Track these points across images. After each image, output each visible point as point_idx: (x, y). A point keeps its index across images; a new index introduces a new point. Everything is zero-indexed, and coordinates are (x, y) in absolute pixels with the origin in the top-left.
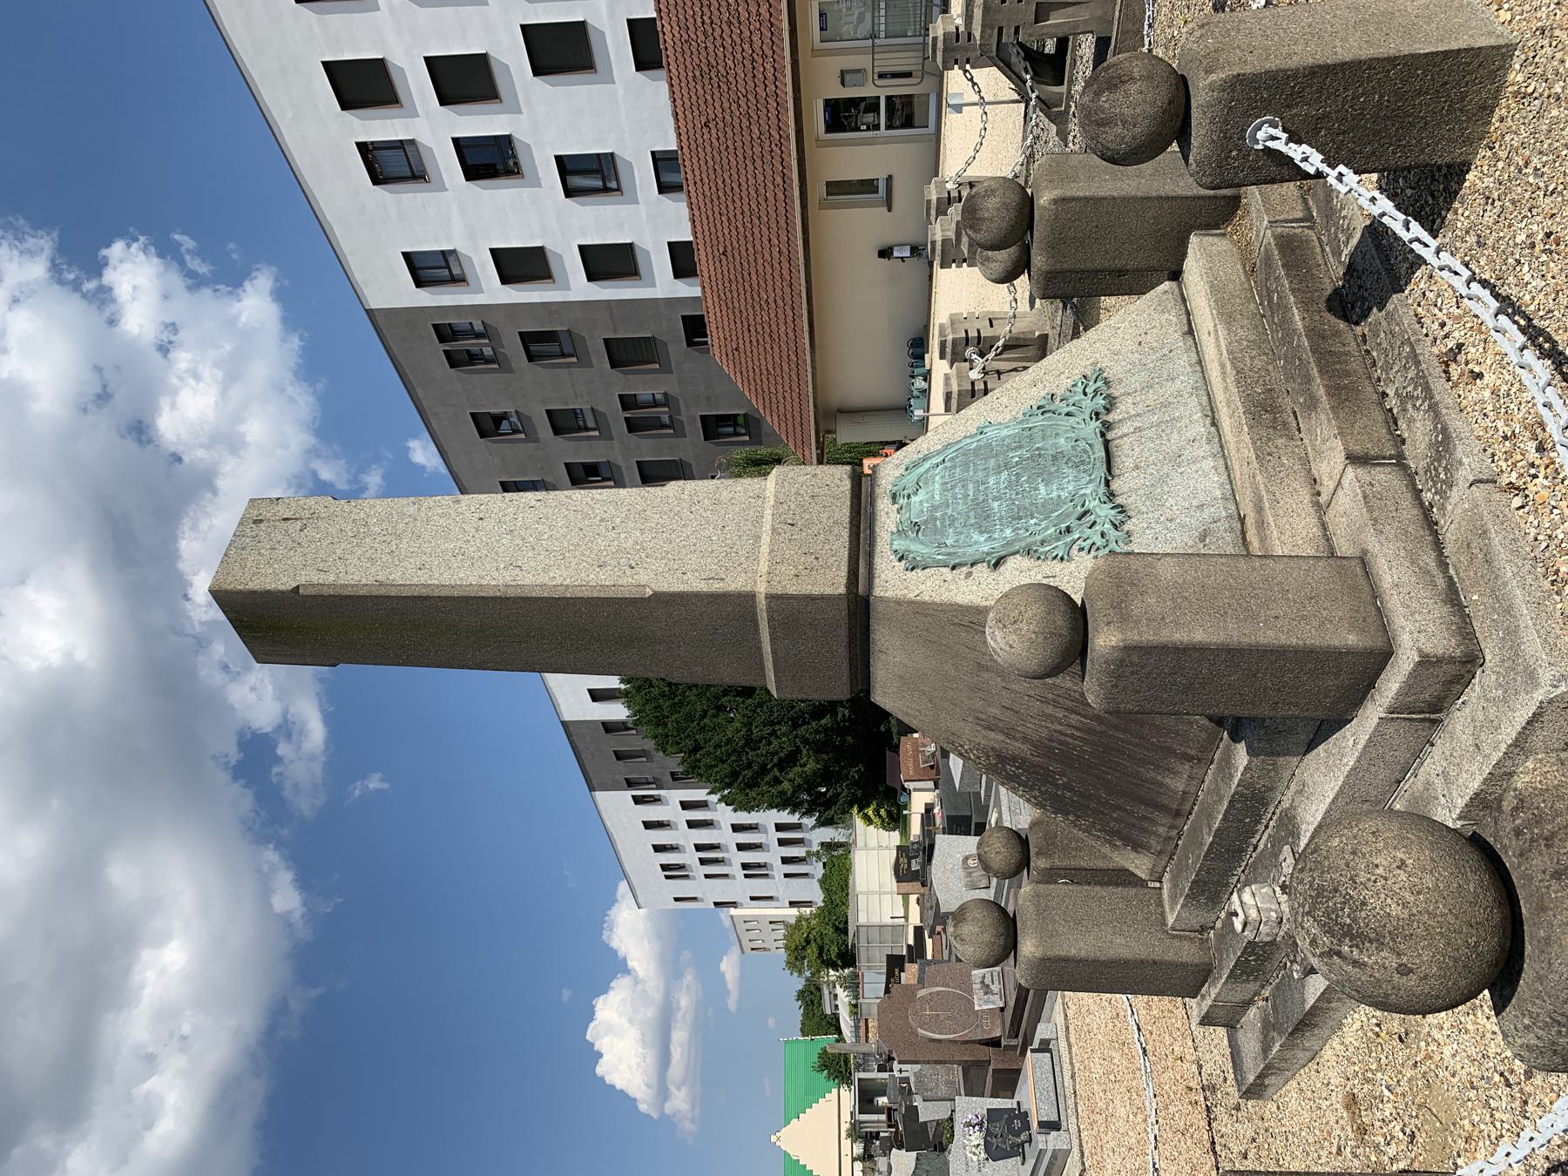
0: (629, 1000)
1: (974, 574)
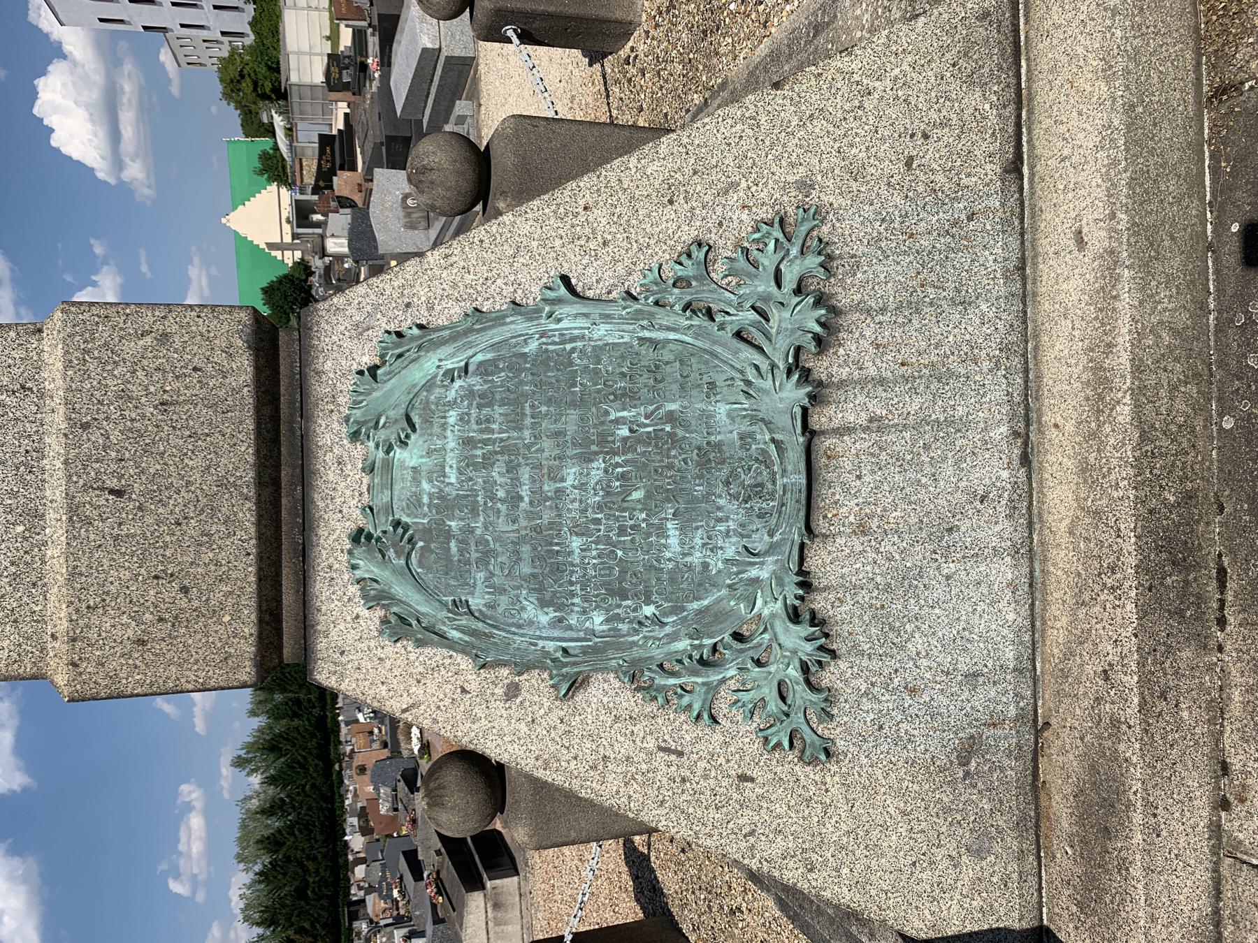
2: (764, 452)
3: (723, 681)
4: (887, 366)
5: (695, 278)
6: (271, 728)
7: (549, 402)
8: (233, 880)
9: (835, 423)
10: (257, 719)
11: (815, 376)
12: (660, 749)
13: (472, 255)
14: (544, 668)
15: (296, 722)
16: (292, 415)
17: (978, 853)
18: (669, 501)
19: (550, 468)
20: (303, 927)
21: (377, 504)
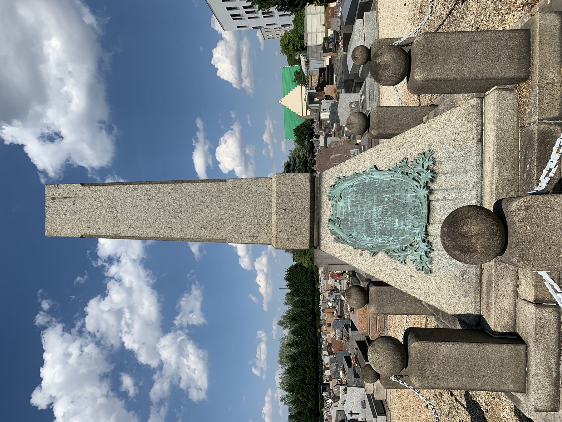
0: (225, 49)
2: (418, 205)
3: (408, 255)
4: (447, 186)
5: (404, 166)
6: (293, 311)
7: (370, 193)
8: (277, 372)
9: (436, 199)
10: (288, 306)
11: (431, 188)
12: (393, 269)
13: (355, 161)
14: (368, 250)
15: (303, 310)
16: (317, 195)
17: (465, 296)
18: (396, 215)
19: (370, 207)
20: (304, 395)
21: (334, 214)
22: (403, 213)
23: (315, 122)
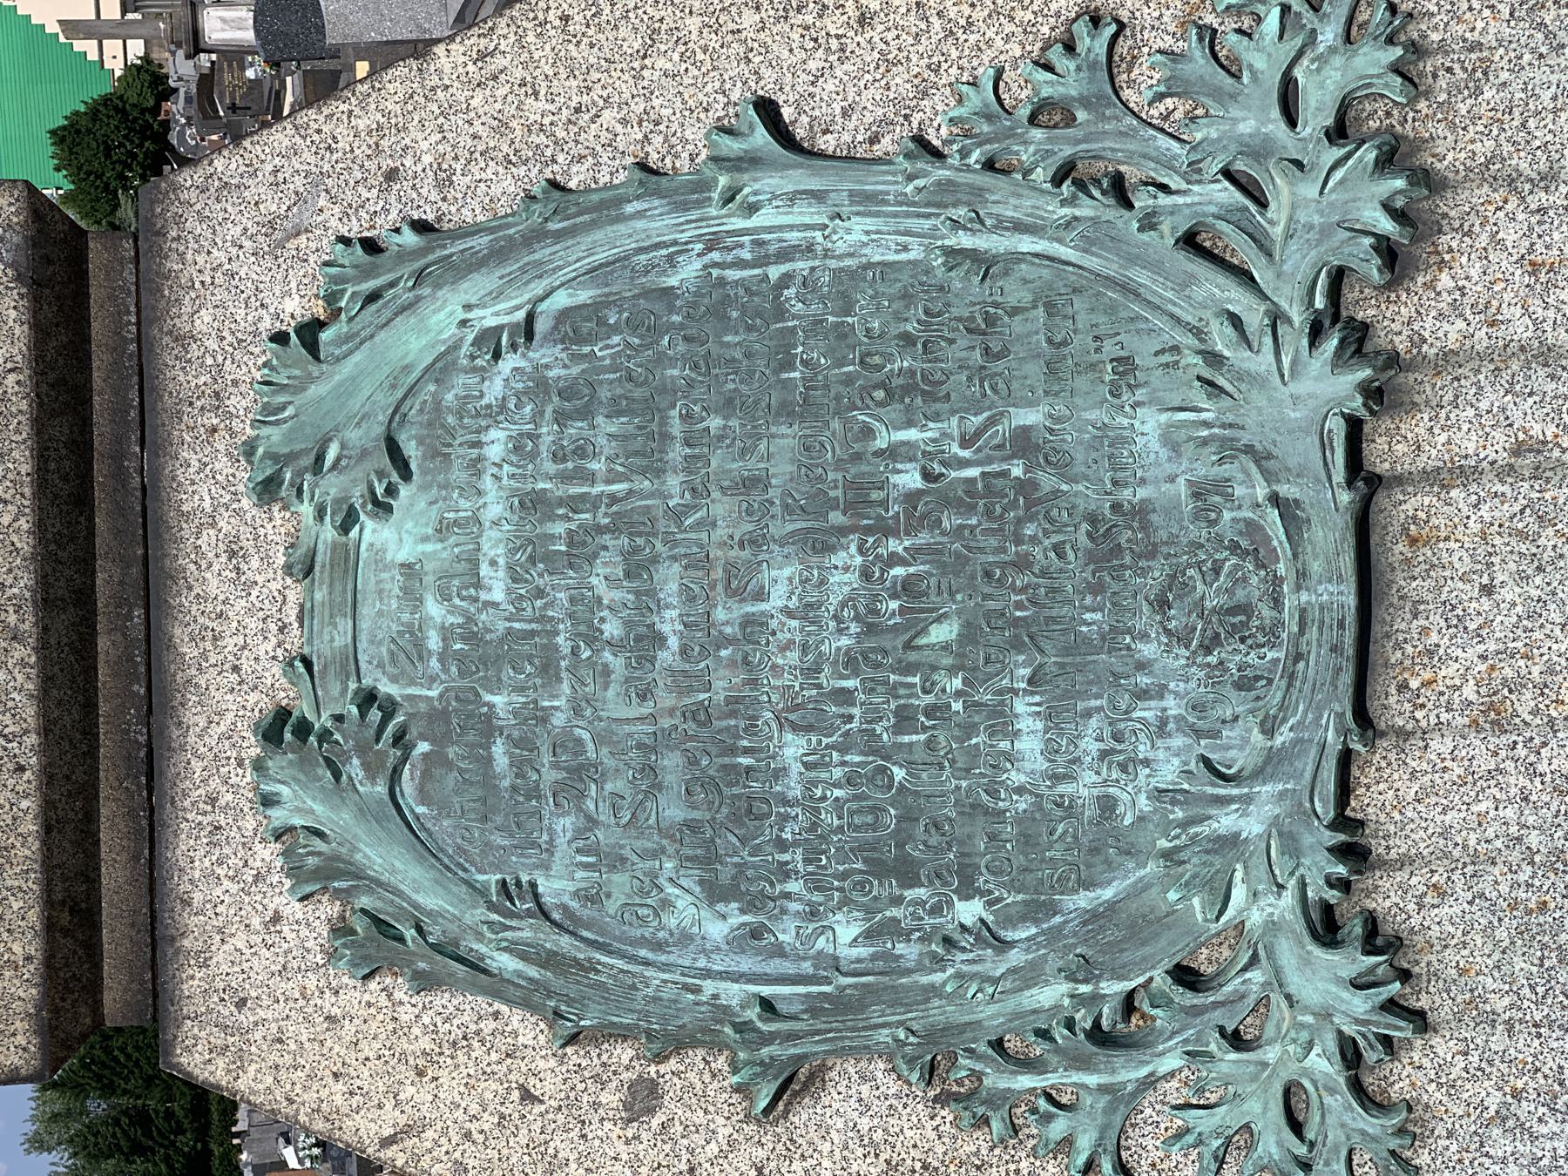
1: (670, 1107)
2: (1252, 528)
3: (1150, 1082)
5: (1085, 102)
7: (728, 405)
9: (1431, 458)
11: (1380, 340)
13: (542, 54)
16: (119, 440)
18: (1017, 645)
19: (730, 567)
22: (1095, 620)
23: (176, 90)
